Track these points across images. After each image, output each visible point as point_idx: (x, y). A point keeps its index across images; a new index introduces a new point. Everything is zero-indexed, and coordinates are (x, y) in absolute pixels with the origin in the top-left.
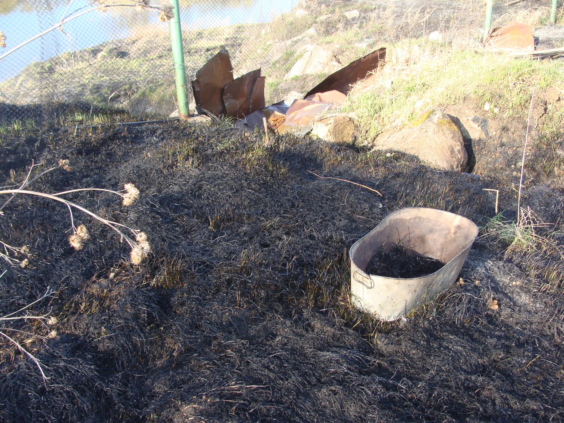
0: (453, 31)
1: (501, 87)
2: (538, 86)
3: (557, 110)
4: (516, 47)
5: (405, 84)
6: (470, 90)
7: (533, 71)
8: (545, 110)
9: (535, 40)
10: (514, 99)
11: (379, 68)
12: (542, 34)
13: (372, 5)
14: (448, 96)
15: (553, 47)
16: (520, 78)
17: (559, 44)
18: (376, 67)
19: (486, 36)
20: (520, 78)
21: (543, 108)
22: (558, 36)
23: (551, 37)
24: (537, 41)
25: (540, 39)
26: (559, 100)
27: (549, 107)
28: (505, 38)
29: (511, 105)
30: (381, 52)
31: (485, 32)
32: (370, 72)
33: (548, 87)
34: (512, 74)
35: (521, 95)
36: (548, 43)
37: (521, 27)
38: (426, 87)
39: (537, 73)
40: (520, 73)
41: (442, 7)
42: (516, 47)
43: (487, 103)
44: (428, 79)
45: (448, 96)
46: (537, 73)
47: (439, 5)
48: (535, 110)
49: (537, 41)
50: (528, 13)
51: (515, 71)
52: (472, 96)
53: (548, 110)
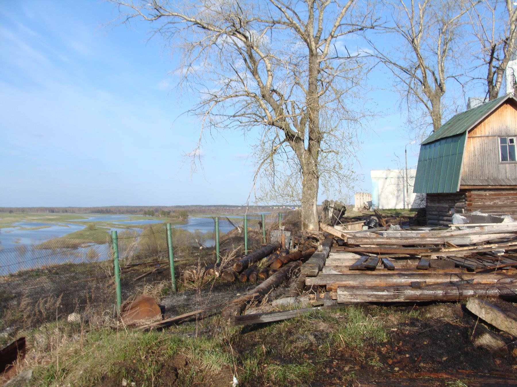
0: (89, 310)
1: (134, 361)
2: (167, 356)
3: (187, 374)
4: (147, 318)
5: (46, 372)
6: (106, 369)
7: (160, 342)
8: (177, 375)
9: (161, 309)
10: (147, 371)
11: (19, 357)
12: (167, 303)
13: (11, 293)
14: (87, 379)
15: (178, 314)
16: (150, 351)
17: (182, 310)
18: (15, 358)
19: (119, 311)
20: (149, 351)
21: (174, 374)
22: (180, 303)
23: (175, 304)
24: (163, 310)
25: (166, 307)
26: (187, 364)
27: (180, 372)
28: (136, 311)
29: (146, 377)
30: (20, 342)
31: (118, 308)
32: (9, 365)
33: (175, 355)
34: (142, 348)
35: (153, 367)
36: (173, 310)
37: (148, 301)
38: (66, 372)
39: (164, 344)
40: (149, 346)
41: (78, 288)
42: (147, 318)
43: (124, 379)
44: (67, 364)
45: (87, 379)
46: (164, 344)
47: (75, 287)
48: (168, 378)
49: (163, 310)
50: (152, 287)
51: (144, 344)
52: (109, 374)
53: (179, 376)
